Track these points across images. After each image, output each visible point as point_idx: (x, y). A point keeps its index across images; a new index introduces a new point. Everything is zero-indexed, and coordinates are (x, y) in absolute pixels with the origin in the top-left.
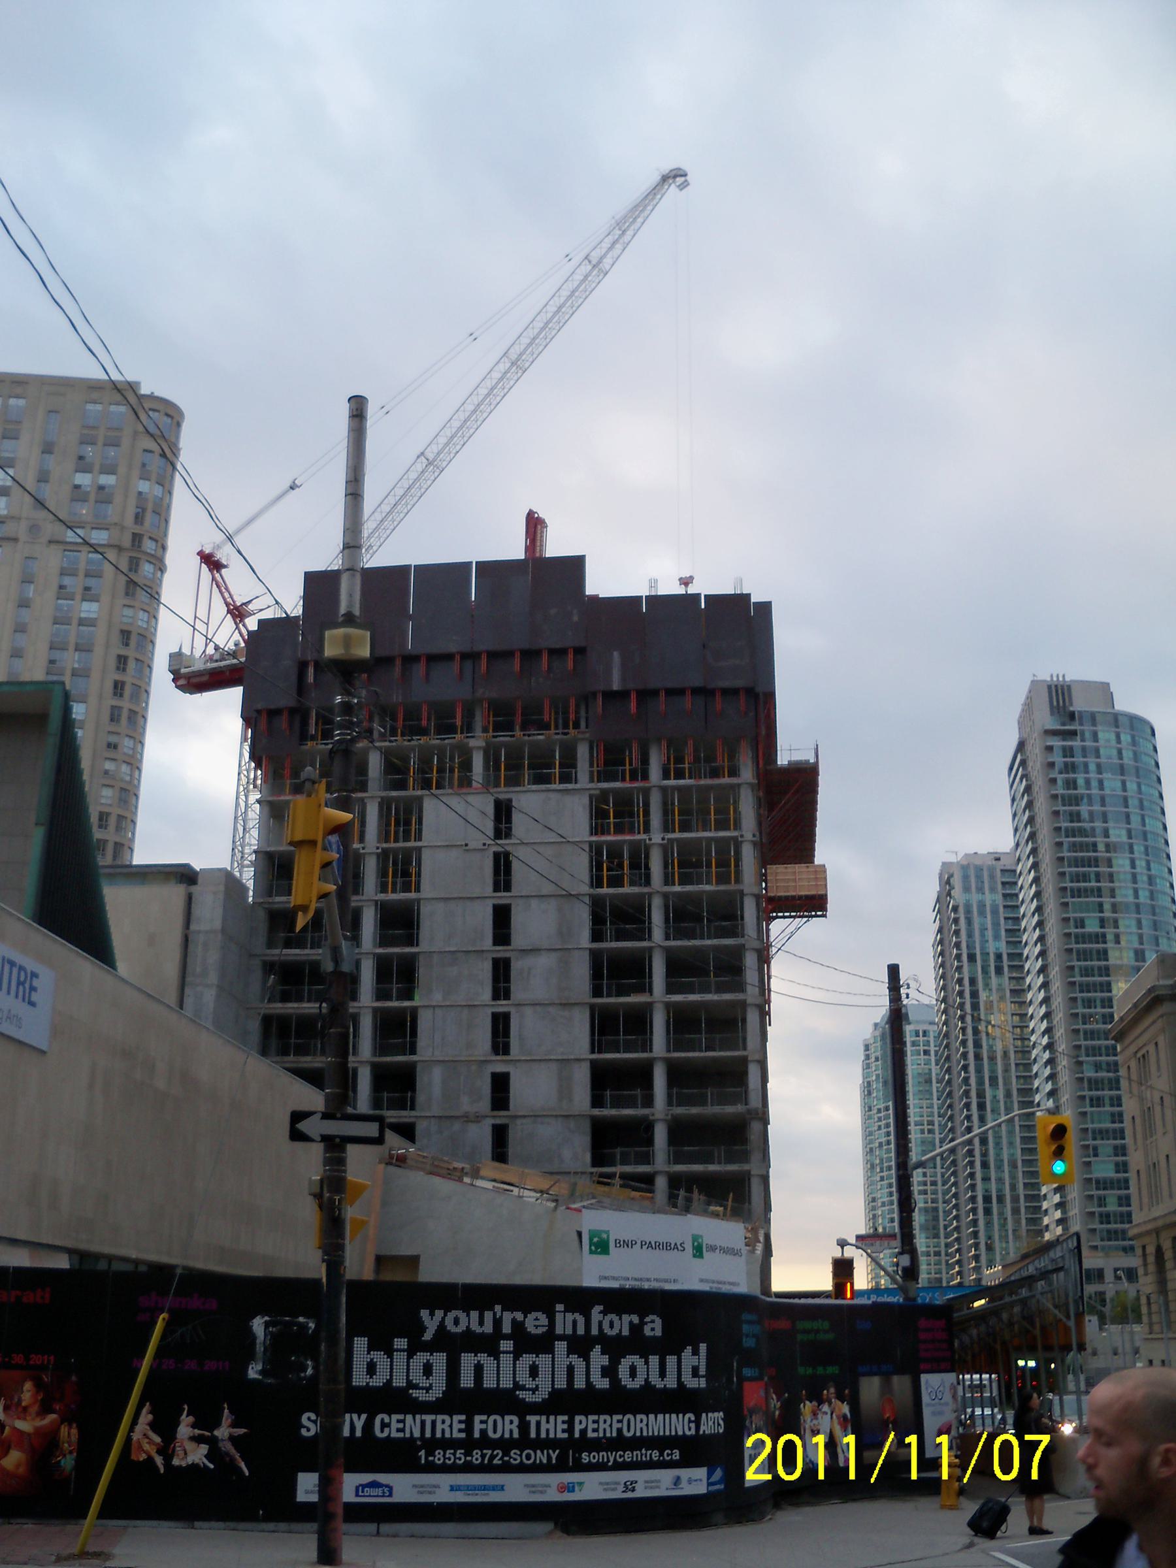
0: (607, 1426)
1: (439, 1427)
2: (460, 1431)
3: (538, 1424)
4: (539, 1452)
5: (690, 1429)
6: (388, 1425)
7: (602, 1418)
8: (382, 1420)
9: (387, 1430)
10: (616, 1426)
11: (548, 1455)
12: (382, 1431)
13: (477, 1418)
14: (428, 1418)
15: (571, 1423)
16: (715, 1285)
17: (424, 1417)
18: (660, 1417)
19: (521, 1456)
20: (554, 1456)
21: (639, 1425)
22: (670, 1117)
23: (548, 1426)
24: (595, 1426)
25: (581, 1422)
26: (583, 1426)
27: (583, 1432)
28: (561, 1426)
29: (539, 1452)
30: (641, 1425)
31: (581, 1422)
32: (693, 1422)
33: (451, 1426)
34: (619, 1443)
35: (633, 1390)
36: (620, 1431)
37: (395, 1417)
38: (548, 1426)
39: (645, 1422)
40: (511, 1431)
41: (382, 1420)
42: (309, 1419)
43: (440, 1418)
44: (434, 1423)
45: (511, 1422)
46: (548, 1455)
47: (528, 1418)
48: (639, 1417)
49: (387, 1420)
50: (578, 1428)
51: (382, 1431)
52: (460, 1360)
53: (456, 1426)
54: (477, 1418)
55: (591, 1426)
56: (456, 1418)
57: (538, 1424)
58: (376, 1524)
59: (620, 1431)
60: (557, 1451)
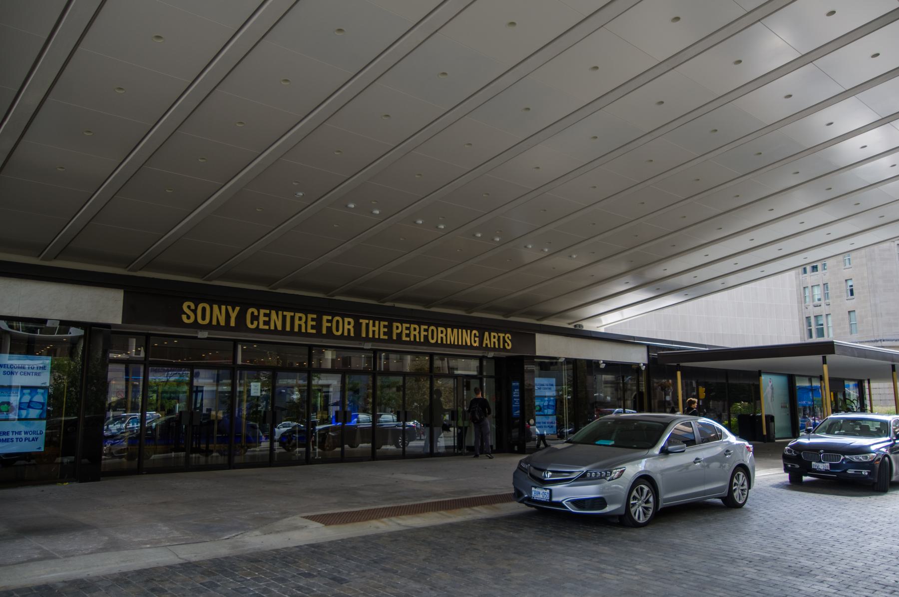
0: (416, 333)
3: (367, 325)
4: (215, 307)
5: (475, 342)
7: (413, 326)
8: (253, 313)
9: (256, 323)
12: (252, 323)
13: (325, 318)
14: (288, 314)
15: (390, 327)
16: (703, 447)
17: (285, 313)
18: (455, 331)
19: (195, 311)
21: (440, 335)
23: (374, 329)
24: (408, 332)
25: (397, 328)
26: (399, 331)
27: (399, 335)
28: (383, 330)
30: (442, 335)
31: (397, 328)
32: (477, 337)
33: (306, 323)
35: (510, 334)
36: (426, 337)
37: (262, 311)
38: (374, 329)
40: (349, 330)
41: (253, 313)
42: (189, 307)
43: (298, 315)
44: (292, 318)
47: (361, 321)
48: (440, 329)
49: (256, 313)
50: (395, 331)
51: (252, 323)
53: (310, 323)
54: (325, 318)
55: (405, 332)
56: (310, 316)
57: (367, 325)
59: (426, 337)
60: (238, 309)
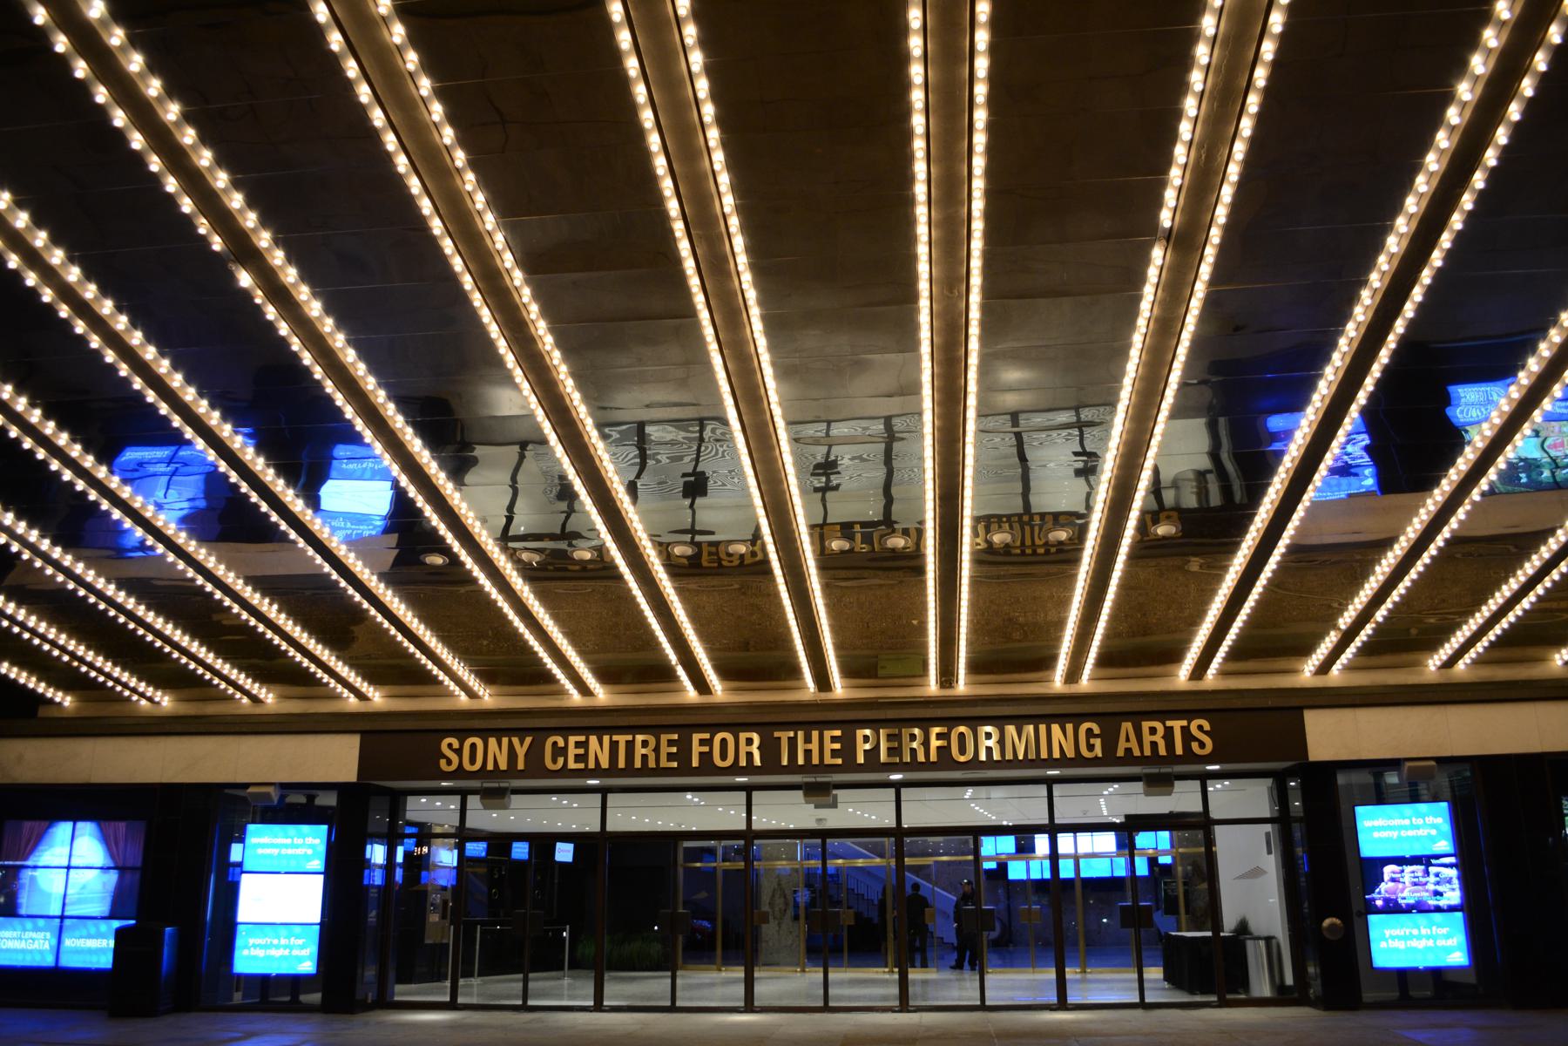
1: (640, 751)
2: (670, 757)
3: (793, 742)
4: (492, 741)
6: (563, 751)
8: (555, 743)
10: (935, 743)
11: (511, 745)
12: (554, 761)
14: (622, 739)
19: (459, 752)
20: (521, 751)
22: (1345, 595)
29: (492, 741)
31: (866, 739)
32: (1096, 736)
34: (998, 1000)
39: (995, 738)
42: (450, 745)
44: (630, 745)
45: (750, 742)
46: (511, 745)
49: (561, 743)
51: (554, 761)
52: (1058, 998)
58: (610, 827)
